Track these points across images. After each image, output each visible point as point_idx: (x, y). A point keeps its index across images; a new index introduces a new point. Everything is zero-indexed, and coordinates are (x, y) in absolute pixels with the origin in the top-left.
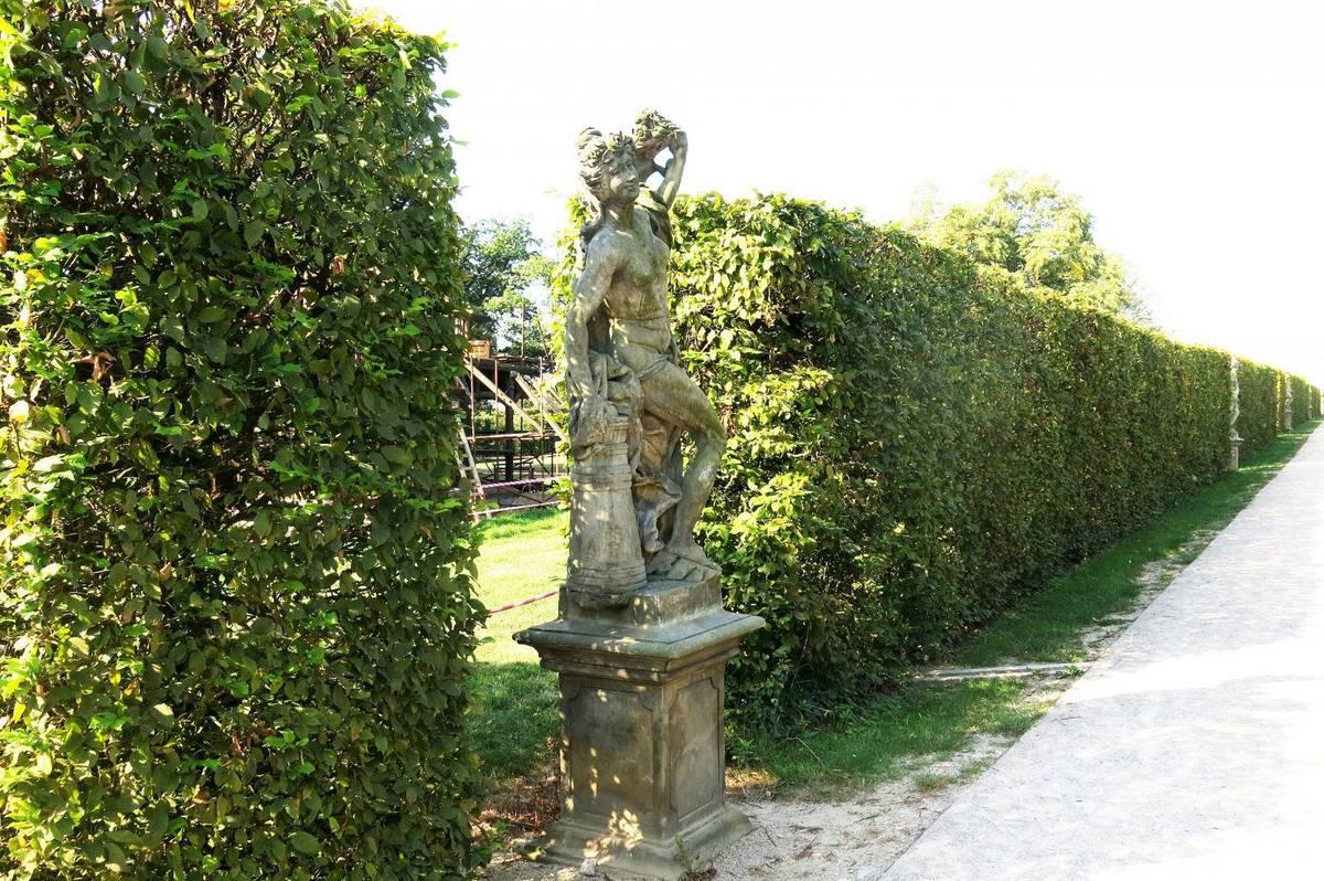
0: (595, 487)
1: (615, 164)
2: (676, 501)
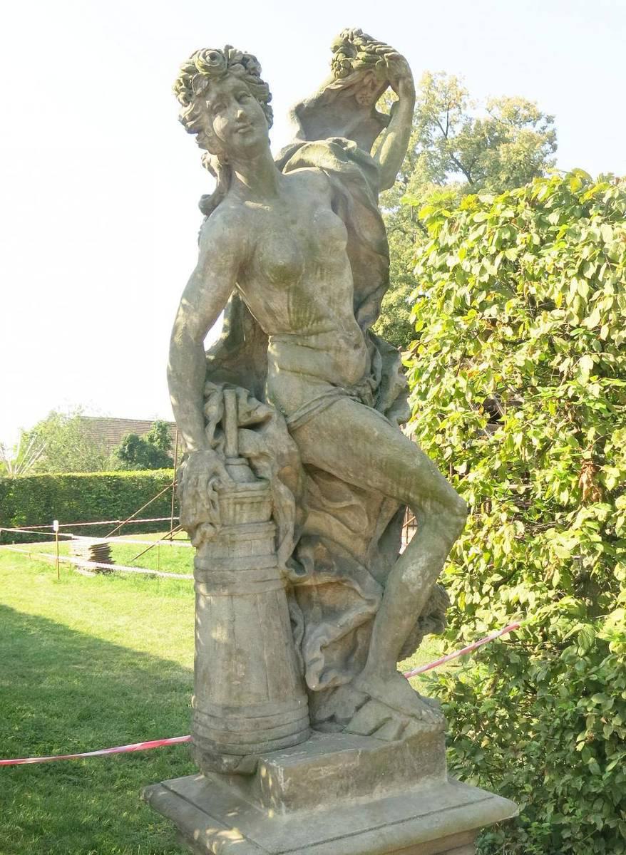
0: (209, 589)
1: (213, 95)
2: (371, 609)
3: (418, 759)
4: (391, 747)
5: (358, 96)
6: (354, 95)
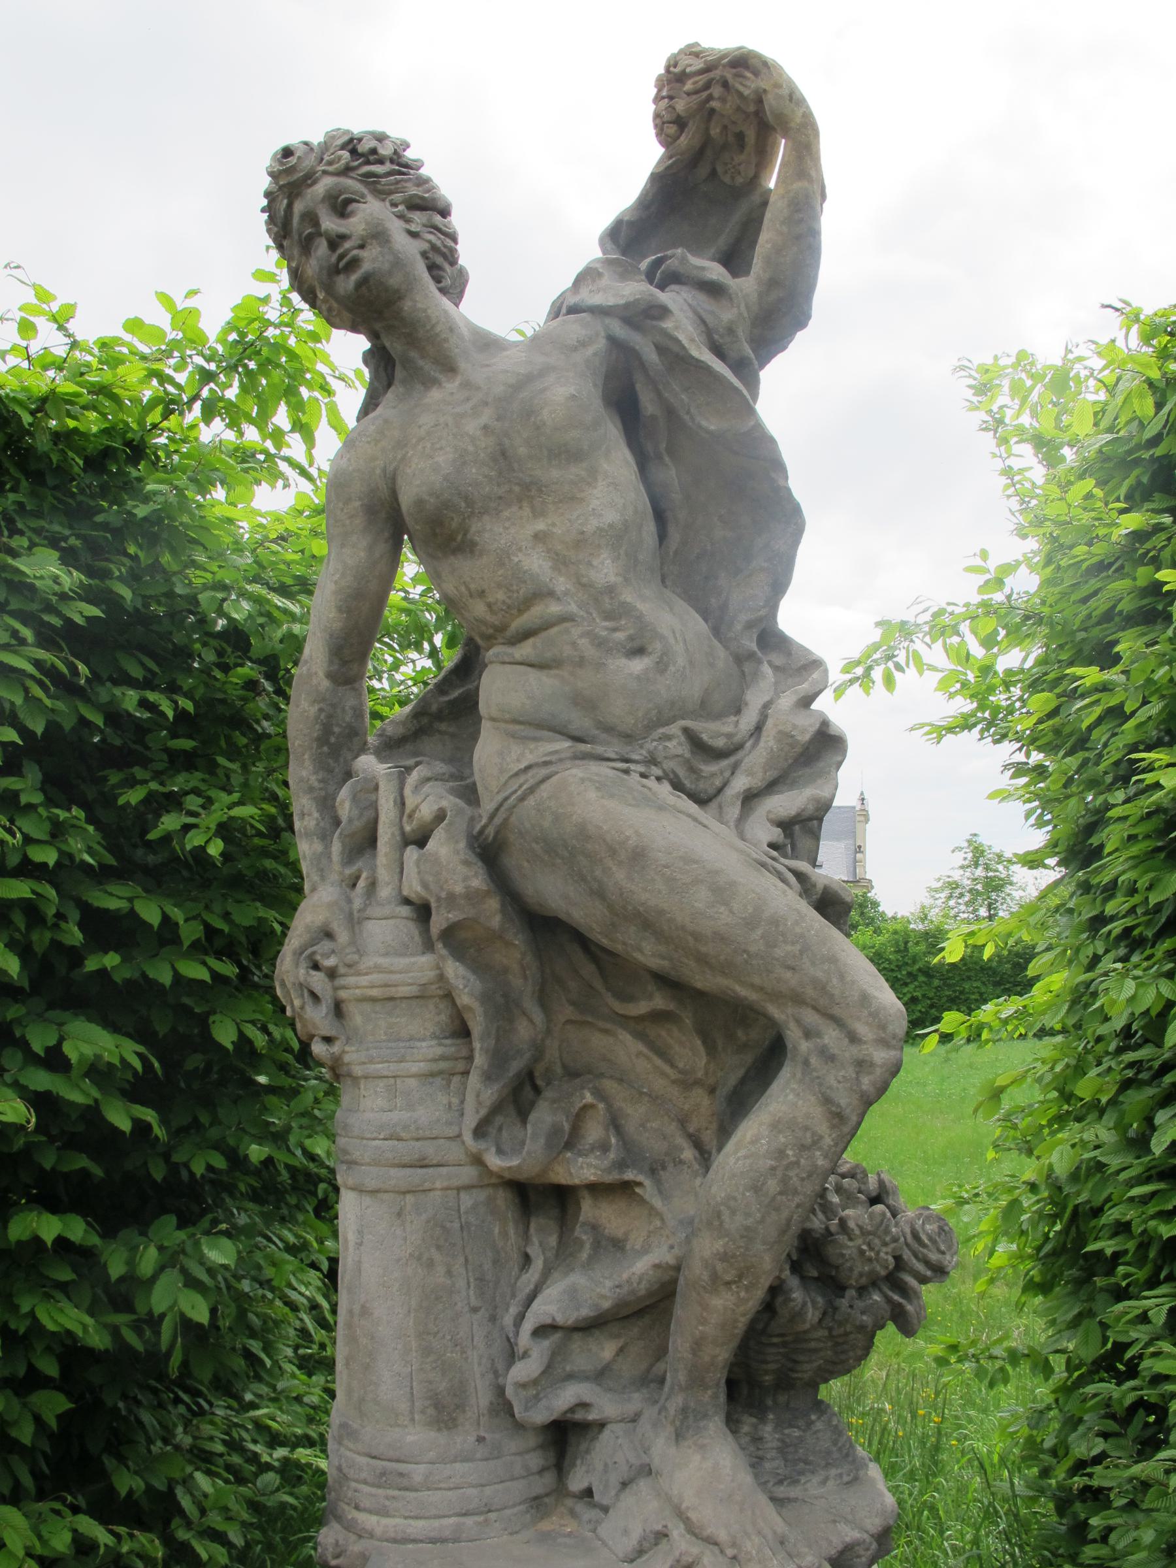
5: (720, 169)
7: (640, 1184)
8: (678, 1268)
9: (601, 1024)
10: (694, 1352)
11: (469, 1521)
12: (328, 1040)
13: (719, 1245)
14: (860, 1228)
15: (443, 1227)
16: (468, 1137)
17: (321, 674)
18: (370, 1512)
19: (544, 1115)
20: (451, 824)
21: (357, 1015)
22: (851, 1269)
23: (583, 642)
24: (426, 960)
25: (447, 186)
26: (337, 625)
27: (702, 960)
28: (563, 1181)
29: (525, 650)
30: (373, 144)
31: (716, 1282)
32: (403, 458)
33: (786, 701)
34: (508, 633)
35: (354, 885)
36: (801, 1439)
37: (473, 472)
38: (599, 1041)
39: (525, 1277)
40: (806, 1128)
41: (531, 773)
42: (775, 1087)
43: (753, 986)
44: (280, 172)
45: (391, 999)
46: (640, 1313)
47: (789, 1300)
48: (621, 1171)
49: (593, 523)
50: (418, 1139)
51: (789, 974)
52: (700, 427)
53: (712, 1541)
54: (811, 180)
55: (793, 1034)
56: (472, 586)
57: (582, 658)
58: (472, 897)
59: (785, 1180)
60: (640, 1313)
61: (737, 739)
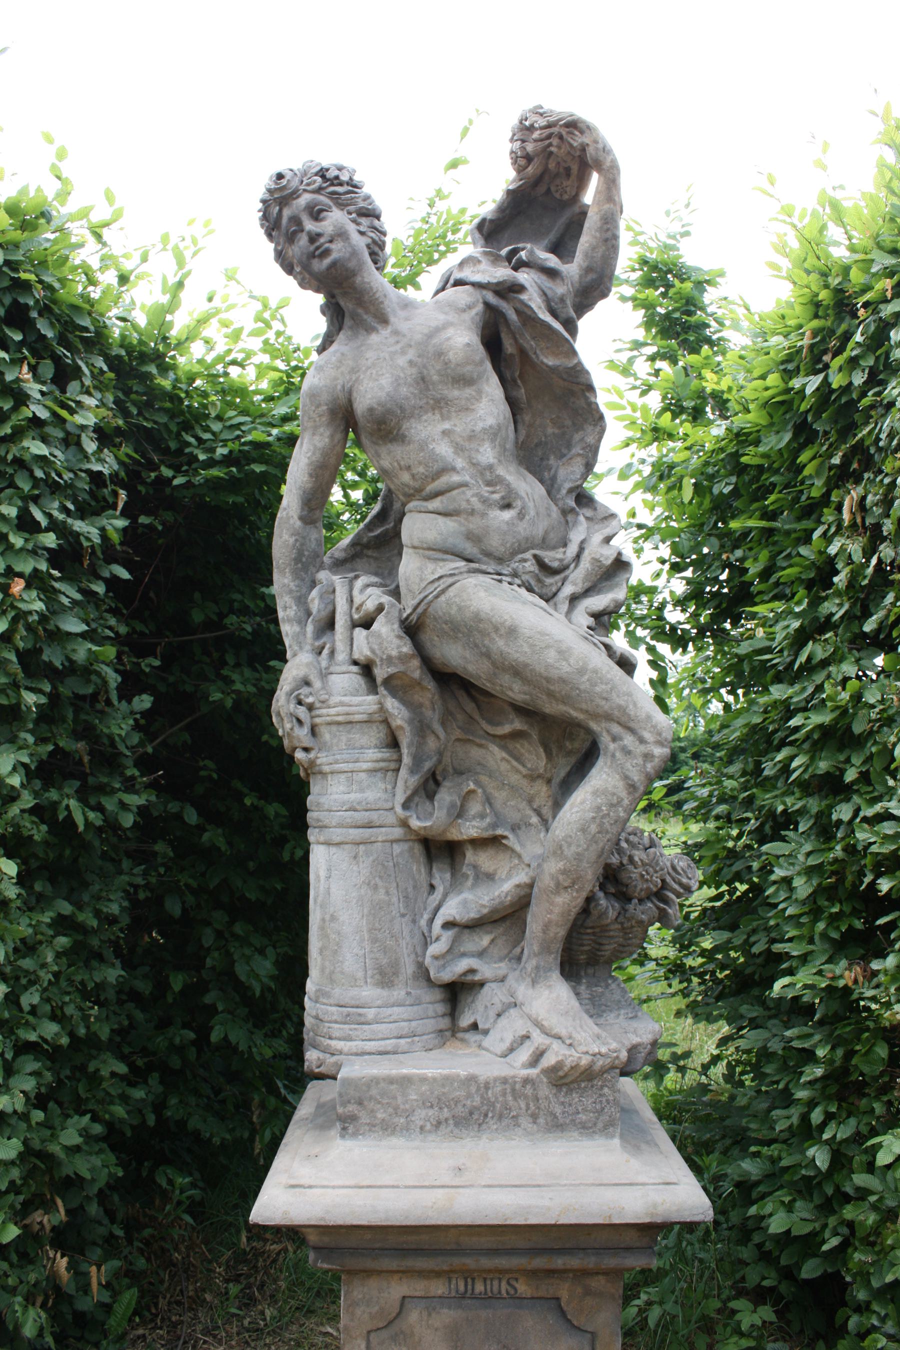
3: (563, 1103)
4: (514, 1077)
5: (553, 189)
6: (549, 190)
7: (505, 837)
8: (531, 886)
9: (477, 740)
10: (544, 932)
11: (402, 1041)
12: (306, 750)
13: (561, 865)
14: (641, 860)
15: (383, 865)
16: (399, 809)
17: (296, 517)
18: (339, 1039)
19: (446, 796)
20: (388, 613)
21: (326, 734)
22: (636, 886)
23: (474, 500)
24: (371, 698)
25: (380, 202)
26: (309, 485)
27: (551, 694)
28: (456, 838)
29: (435, 504)
30: (336, 173)
31: (559, 888)
32: (357, 379)
33: (597, 538)
34: (424, 494)
35: (320, 653)
36: (603, 993)
37: (404, 391)
38: (475, 753)
39: (431, 898)
40: (614, 794)
41: (442, 581)
42: (594, 771)
43: (581, 710)
44: (276, 189)
45: (351, 722)
46: (503, 919)
47: (598, 905)
48: (494, 830)
49: (480, 425)
50: (367, 810)
51: (604, 702)
52: (542, 363)
53: (558, 1037)
54: (615, 204)
55: (605, 740)
56: (402, 463)
57: (473, 510)
58: (403, 658)
59: (601, 825)
60: (503, 919)
61: (566, 562)
